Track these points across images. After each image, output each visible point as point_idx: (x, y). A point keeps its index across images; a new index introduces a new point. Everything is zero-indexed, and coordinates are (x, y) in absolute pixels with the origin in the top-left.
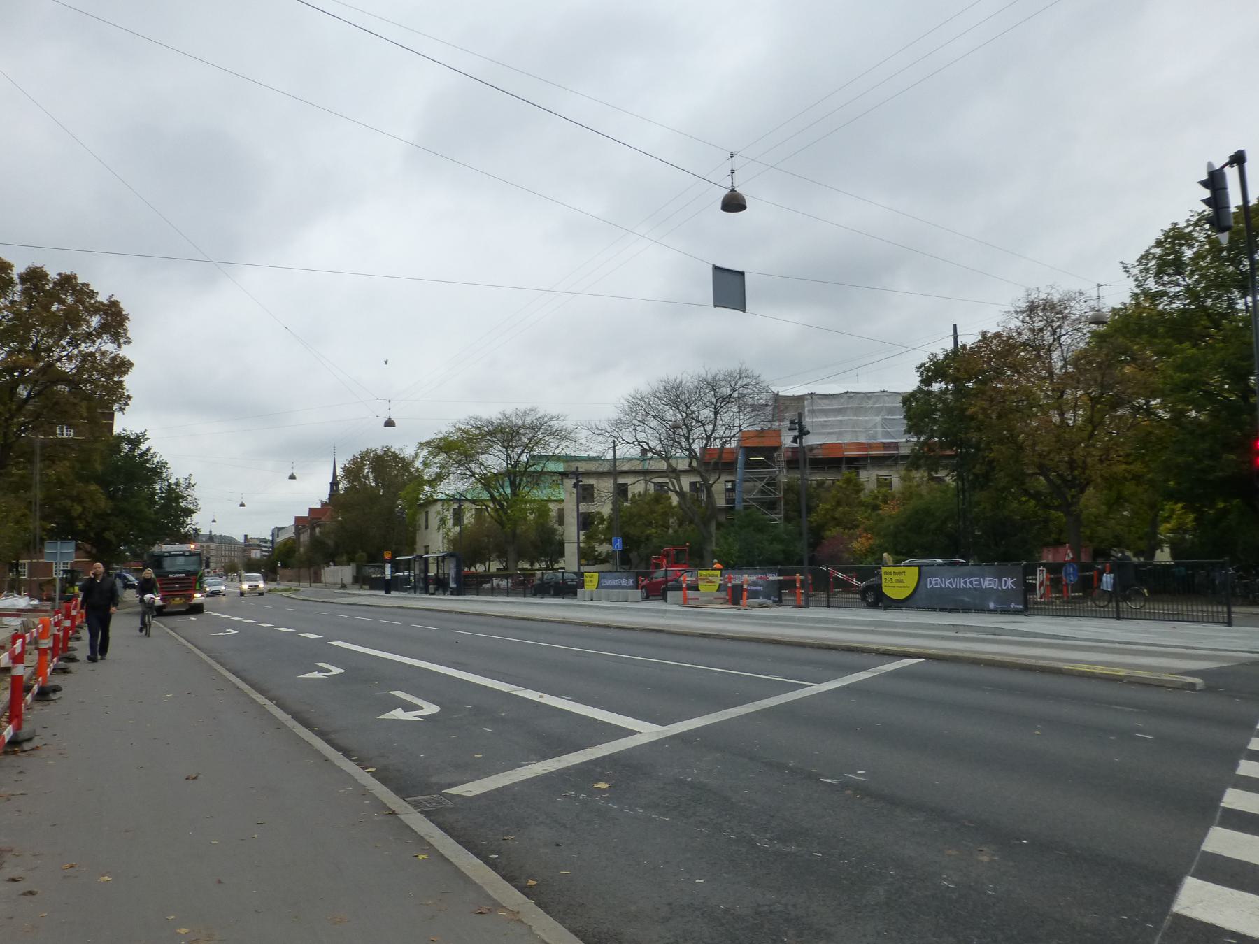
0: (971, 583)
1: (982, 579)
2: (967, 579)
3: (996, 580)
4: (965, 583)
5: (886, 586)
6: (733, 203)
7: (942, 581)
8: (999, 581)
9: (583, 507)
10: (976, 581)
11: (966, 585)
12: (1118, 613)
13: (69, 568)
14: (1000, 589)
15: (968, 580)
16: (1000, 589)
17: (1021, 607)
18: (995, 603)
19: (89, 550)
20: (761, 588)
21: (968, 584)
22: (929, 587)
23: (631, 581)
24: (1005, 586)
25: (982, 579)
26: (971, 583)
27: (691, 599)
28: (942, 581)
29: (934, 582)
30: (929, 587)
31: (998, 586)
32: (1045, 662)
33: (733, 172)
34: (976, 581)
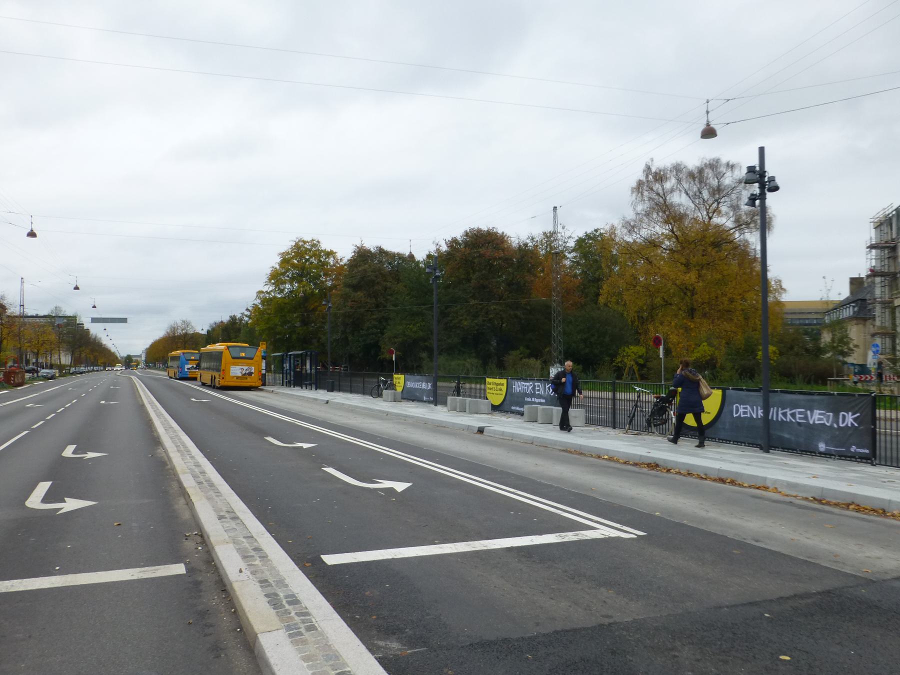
0: (793, 415)
1: (809, 412)
2: (787, 410)
3: (831, 414)
4: (785, 414)
5: (488, 393)
7: (753, 410)
8: (834, 416)
9: (142, 365)
10: (800, 413)
11: (786, 418)
13: (536, 393)
14: (835, 426)
16: (835, 426)
17: (867, 451)
18: (827, 445)
19: (208, 366)
21: (789, 417)
22: (735, 416)
23: (430, 384)
24: (736, 414)
25: (809, 412)
26: (793, 415)
27: (897, 439)
28: (753, 410)
29: (741, 410)
30: (735, 416)
31: (833, 422)
32: (291, 393)
33: (708, 112)
34: (800, 413)
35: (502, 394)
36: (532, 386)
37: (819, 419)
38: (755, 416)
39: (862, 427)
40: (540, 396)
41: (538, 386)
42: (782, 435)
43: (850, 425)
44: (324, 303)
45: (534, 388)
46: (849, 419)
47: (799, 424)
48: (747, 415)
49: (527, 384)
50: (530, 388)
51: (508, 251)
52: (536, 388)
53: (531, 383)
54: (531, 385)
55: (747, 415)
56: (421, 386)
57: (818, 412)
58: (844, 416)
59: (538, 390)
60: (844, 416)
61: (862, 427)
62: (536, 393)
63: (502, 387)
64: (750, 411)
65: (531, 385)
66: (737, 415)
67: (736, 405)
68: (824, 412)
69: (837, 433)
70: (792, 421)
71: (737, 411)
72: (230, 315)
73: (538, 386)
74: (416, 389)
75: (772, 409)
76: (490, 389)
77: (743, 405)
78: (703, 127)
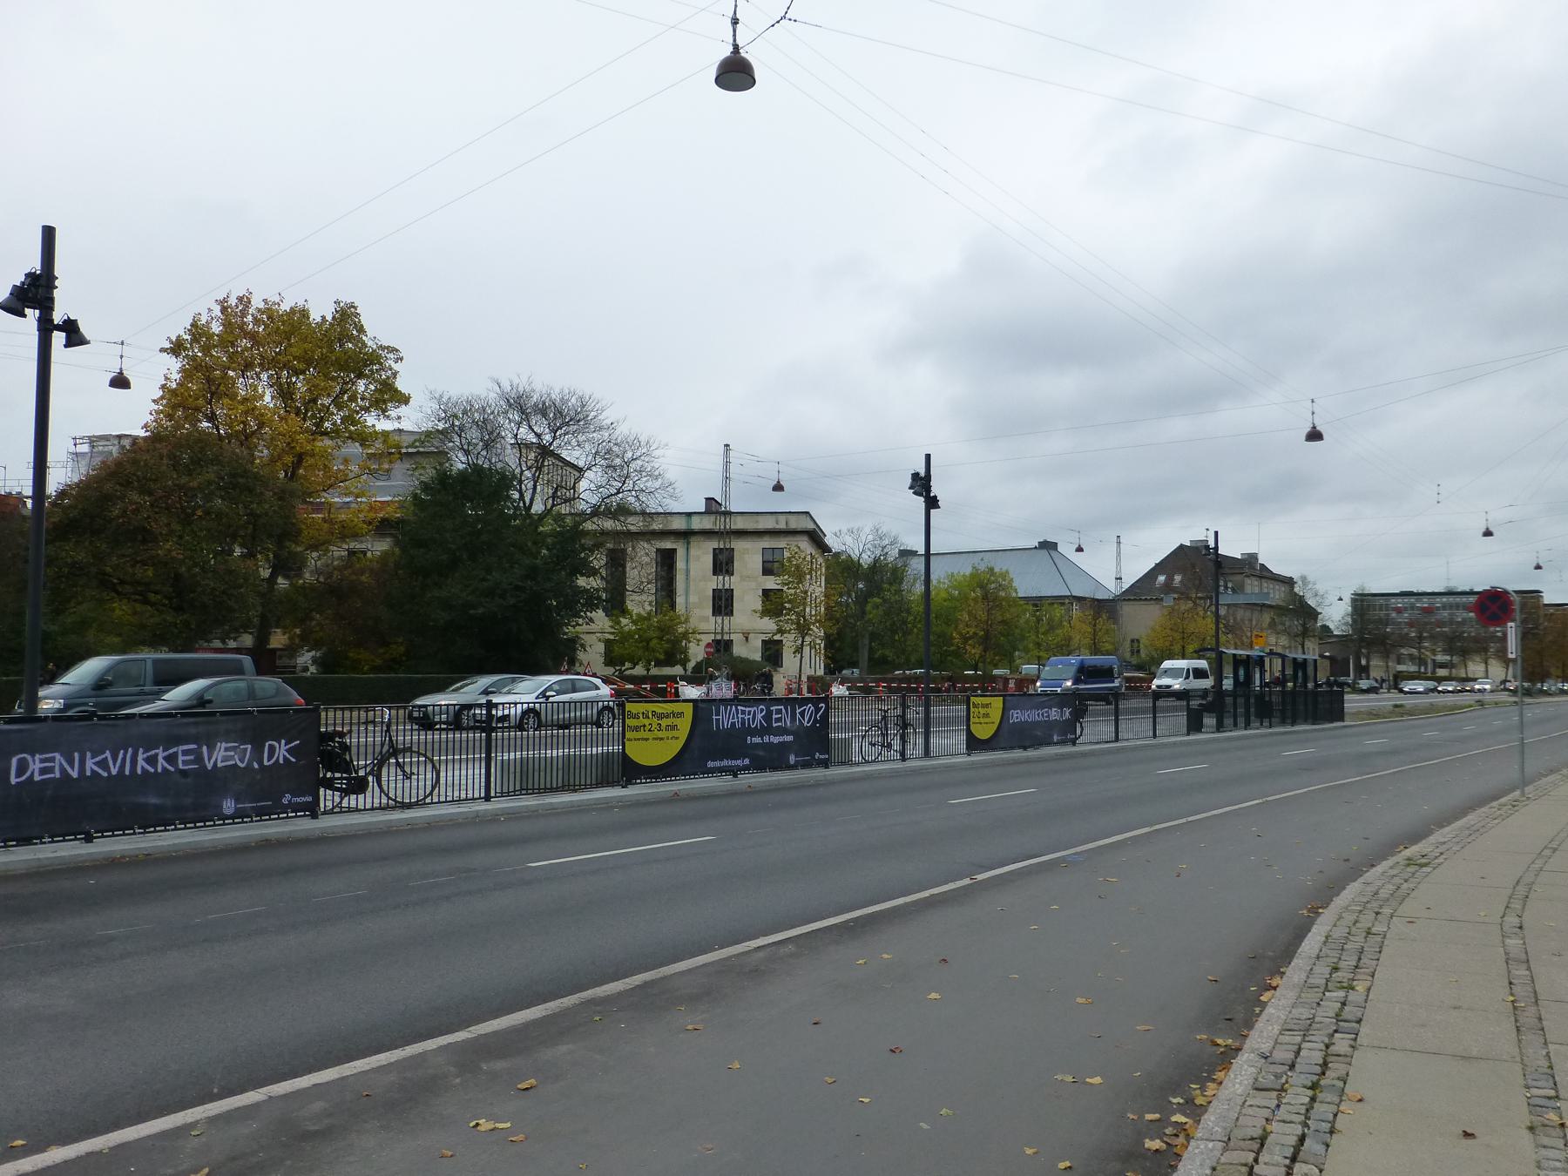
0: (171, 759)
1: (205, 748)
3: (249, 746)
6: (735, 73)
10: (185, 753)
11: (155, 767)
12: (1270, 725)
13: (774, 725)
15: (161, 754)
20: (790, 738)
21: (161, 762)
22: (13, 780)
34: (185, 753)
35: (993, 723)
36: (763, 713)
37: (225, 759)
38: (75, 774)
39: (303, 762)
40: (783, 731)
41: (779, 712)
42: (142, 800)
43: (281, 761)
44: (228, 539)
45: (768, 717)
46: (282, 751)
47: (184, 773)
48: (52, 775)
49: (752, 710)
50: (759, 716)
51: (72, 489)
52: (774, 716)
53: (761, 707)
54: (762, 710)
55: (52, 775)
56: (1048, 716)
57: (224, 745)
58: (272, 749)
59: (778, 720)
60: (272, 749)
61: (303, 762)
62: (774, 725)
63: (677, 721)
64: (61, 764)
65: (762, 710)
66: (272, 762)
67: (270, 742)
68: (236, 744)
69: (259, 777)
70: (168, 770)
71: (22, 768)
72: (1011, 571)
73: (779, 712)
74: (1036, 724)
75: (219, 744)
76: (637, 729)
77: (226, 743)
78: (1484, 530)
